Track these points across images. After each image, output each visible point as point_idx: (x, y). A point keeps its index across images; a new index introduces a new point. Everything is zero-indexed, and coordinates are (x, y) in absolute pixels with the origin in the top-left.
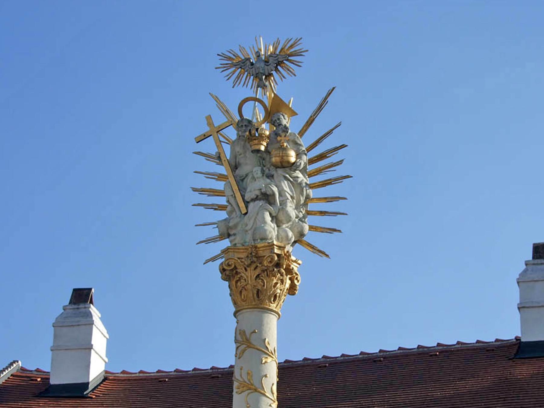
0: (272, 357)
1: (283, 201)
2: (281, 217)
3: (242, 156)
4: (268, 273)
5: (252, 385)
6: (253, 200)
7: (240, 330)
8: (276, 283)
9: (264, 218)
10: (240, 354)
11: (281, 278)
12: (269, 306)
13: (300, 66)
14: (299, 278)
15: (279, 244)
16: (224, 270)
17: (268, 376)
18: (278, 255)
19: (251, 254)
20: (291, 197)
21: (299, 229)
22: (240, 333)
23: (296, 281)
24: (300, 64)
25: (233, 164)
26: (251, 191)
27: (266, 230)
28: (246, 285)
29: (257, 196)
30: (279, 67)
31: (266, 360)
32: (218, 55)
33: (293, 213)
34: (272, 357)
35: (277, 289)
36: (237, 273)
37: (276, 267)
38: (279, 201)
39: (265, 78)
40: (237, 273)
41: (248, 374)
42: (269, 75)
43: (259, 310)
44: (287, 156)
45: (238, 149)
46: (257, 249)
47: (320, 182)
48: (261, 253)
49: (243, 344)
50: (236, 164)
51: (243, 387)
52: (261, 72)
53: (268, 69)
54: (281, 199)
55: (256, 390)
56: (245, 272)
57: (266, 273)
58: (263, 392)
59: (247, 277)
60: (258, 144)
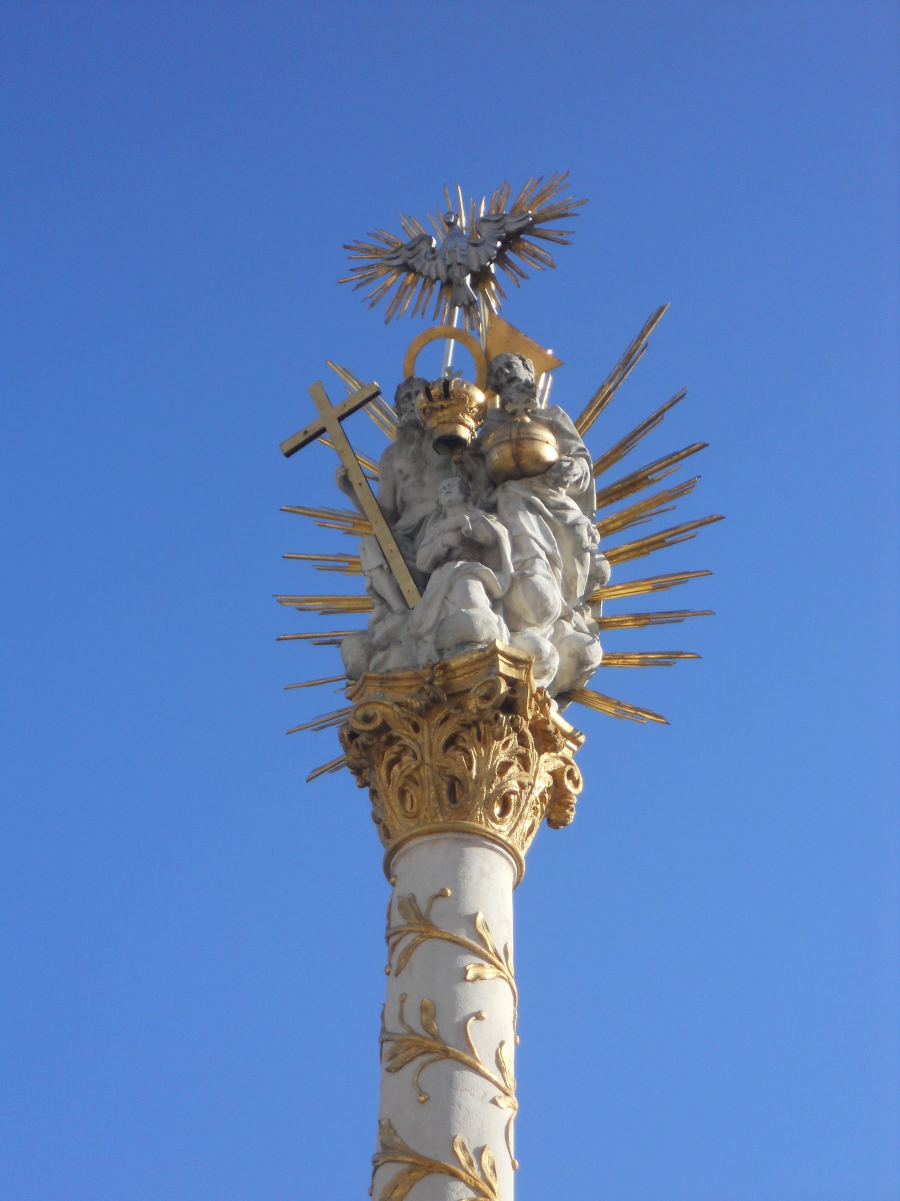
0: (499, 968)
1: (523, 563)
2: (520, 602)
3: (411, 480)
4: (482, 730)
5: (435, 1037)
6: (438, 563)
7: (399, 897)
8: (506, 765)
9: (467, 593)
10: (400, 958)
11: (522, 750)
12: (487, 825)
13: (565, 243)
14: (577, 774)
15: (514, 652)
16: (353, 735)
17: (484, 1015)
18: (511, 682)
19: (430, 683)
20: (549, 556)
21: (574, 646)
22: (400, 907)
23: (569, 784)
24: (565, 238)
25: (388, 504)
26: (432, 541)
27: (469, 619)
28: (417, 769)
29: (451, 550)
30: (509, 253)
31: (479, 971)
32: (346, 247)
33: (556, 598)
34: (499, 968)
35: (510, 778)
36: (391, 740)
37: (504, 713)
38: (514, 564)
39: (474, 285)
40: (391, 740)
41: (423, 1009)
42: (481, 277)
43: (456, 835)
44: (533, 439)
45: (401, 464)
46: (449, 675)
47: (618, 483)
48: (460, 682)
49: (409, 932)
50: (395, 503)
51: (409, 1048)
52: (459, 260)
53: (479, 258)
54: (518, 558)
55: (446, 1054)
56: (414, 735)
57: (474, 730)
58: (467, 1058)
59: (420, 747)
60: (450, 422)
